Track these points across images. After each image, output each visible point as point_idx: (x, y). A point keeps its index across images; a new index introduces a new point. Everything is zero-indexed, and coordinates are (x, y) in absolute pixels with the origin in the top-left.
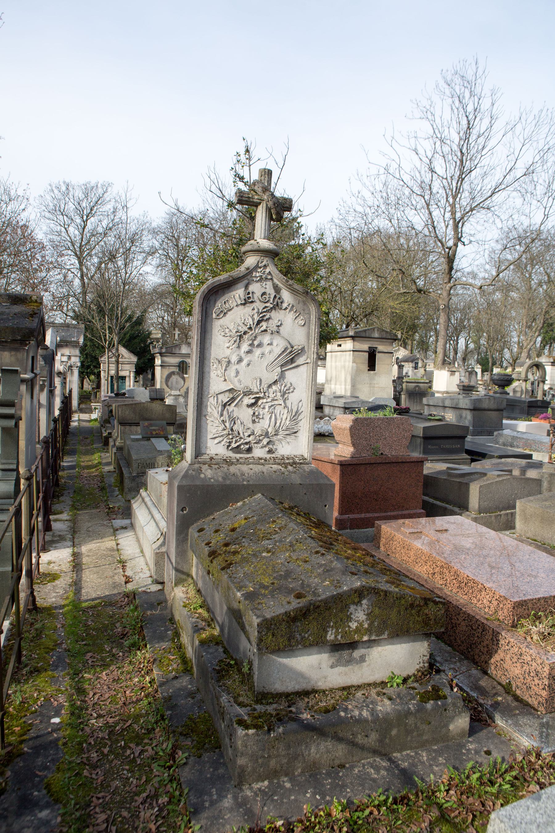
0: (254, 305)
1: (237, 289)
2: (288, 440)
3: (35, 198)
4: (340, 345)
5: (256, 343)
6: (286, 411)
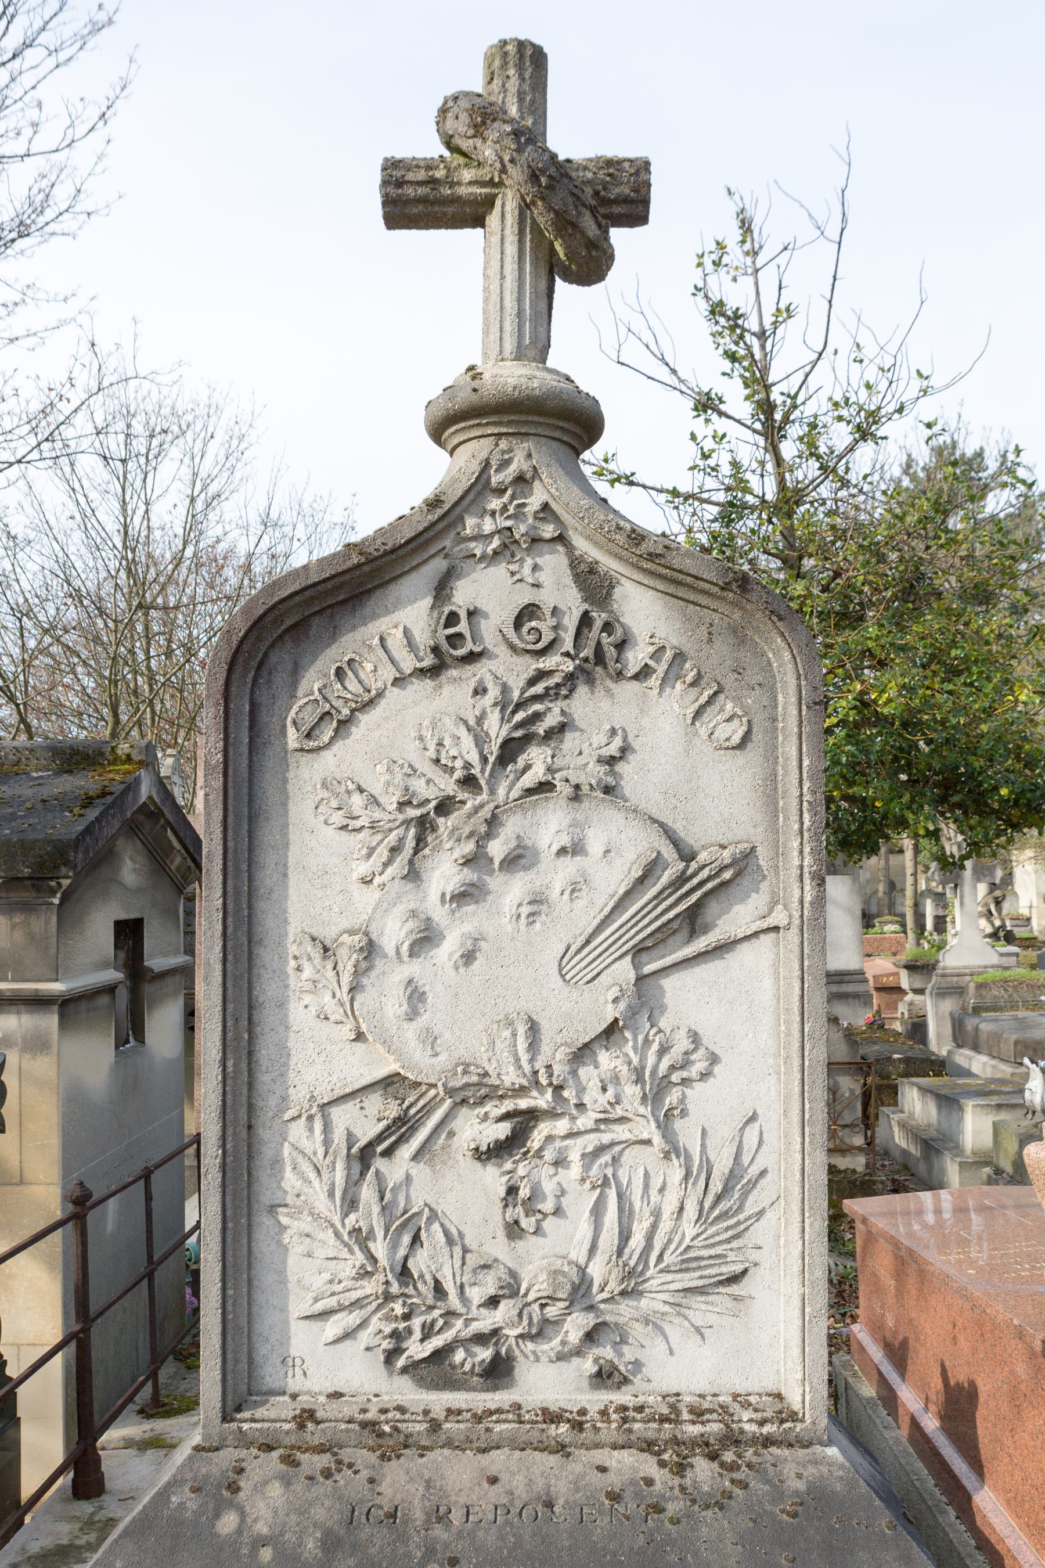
0: (482, 670)
1: (398, 605)
5: (497, 849)
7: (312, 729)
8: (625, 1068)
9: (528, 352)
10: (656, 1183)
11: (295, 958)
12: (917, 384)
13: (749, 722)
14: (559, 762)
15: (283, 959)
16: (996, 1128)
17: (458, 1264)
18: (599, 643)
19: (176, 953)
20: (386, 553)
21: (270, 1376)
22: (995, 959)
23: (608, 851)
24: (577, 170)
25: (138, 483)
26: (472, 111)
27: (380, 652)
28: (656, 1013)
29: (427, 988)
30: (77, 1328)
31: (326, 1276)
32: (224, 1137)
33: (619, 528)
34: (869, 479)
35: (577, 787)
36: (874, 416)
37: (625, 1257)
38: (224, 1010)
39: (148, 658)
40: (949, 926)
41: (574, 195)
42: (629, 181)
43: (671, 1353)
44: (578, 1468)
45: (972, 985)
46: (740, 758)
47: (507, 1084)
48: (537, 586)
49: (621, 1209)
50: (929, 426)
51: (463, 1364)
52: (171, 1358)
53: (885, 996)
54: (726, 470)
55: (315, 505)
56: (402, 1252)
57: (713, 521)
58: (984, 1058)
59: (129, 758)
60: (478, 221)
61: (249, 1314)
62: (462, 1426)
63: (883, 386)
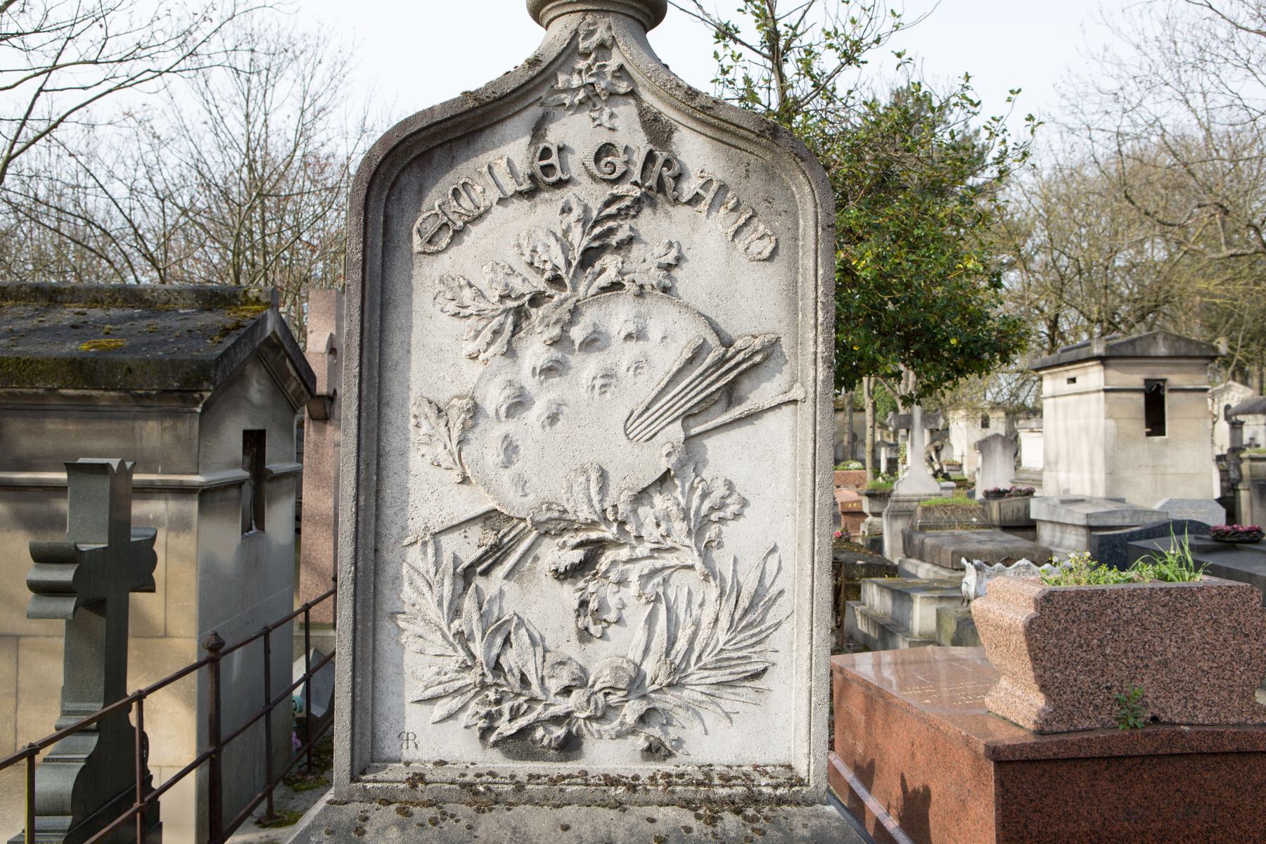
0: (568, 194)
1: (503, 141)
2: (727, 706)
4: (1073, 380)
5: (577, 334)
6: (715, 592)
7: (433, 236)
8: (675, 508)
10: (697, 599)
11: (415, 417)
12: (891, 21)
13: (777, 240)
14: (627, 267)
15: (405, 418)
16: (939, 614)
17: (540, 661)
18: (660, 175)
19: (291, 460)
20: (496, 100)
21: (389, 747)
22: (938, 490)
23: (665, 337)
25: (260, 97)
27: (488, 177)
28: (700, 465)
29: (519, 443)
30: (211, 750)
31: (435, 669)
32: (356, 557)
33: (678, 86)
35: (642, 287)
36: (857, 45)
37: (672, 657)
38: (358, 456)
39: (263, 235)
40: (900, 466)
43: (706, 733)
44: (633, 819)
45: (919, 509)
46: (769, 268)
47: (582, 519)
48: (612, 129)
49: (669, 620)
50: (899, 55)
51: (542, 740)
52: (281, 783)
53: (848, 517)
54: (740, 84)
56: (495, 651)
58: (927, 566)
59: (258, 300)
61: (373, 698)
62: (541, 787)
63: (865, 21)
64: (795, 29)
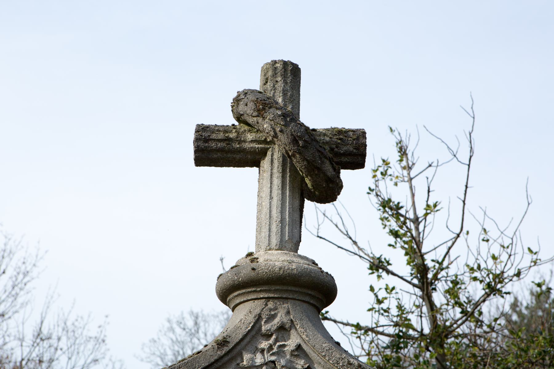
3: (144, 344)
9: (287, 245)
12: (529, 258)
24: (320, 136)
26: (256, 102)
34: (498, 322)
36: (499, 278)
41: (319, 151)
42: (352, 143)
54: (394, 311)
55: (76, 324)
57: (385, 348)
60: (256, 163)
63: (504, 257)
64: (441, 264)
